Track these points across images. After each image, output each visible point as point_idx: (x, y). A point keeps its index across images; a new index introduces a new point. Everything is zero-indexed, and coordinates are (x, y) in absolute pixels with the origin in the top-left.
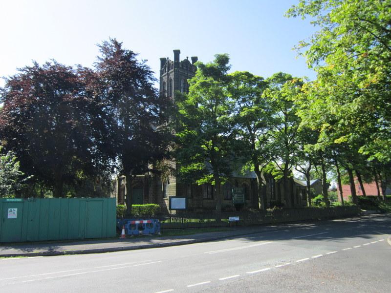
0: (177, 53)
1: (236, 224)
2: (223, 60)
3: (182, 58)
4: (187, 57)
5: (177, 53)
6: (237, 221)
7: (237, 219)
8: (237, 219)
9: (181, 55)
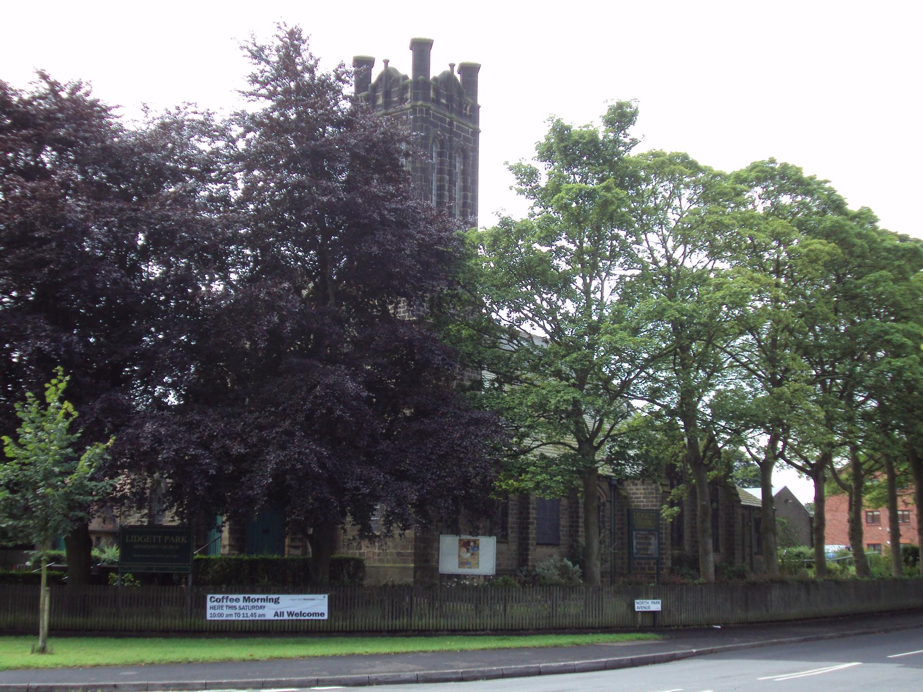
0: (421, 50)
1: (652, 624)
2: (621, 117)
3: (437, 69)
4: (452, 66)
5: (421, 50)
6: (654, 612)
7: (654, 605)
8: (654, 605)
9: (433, 52)
